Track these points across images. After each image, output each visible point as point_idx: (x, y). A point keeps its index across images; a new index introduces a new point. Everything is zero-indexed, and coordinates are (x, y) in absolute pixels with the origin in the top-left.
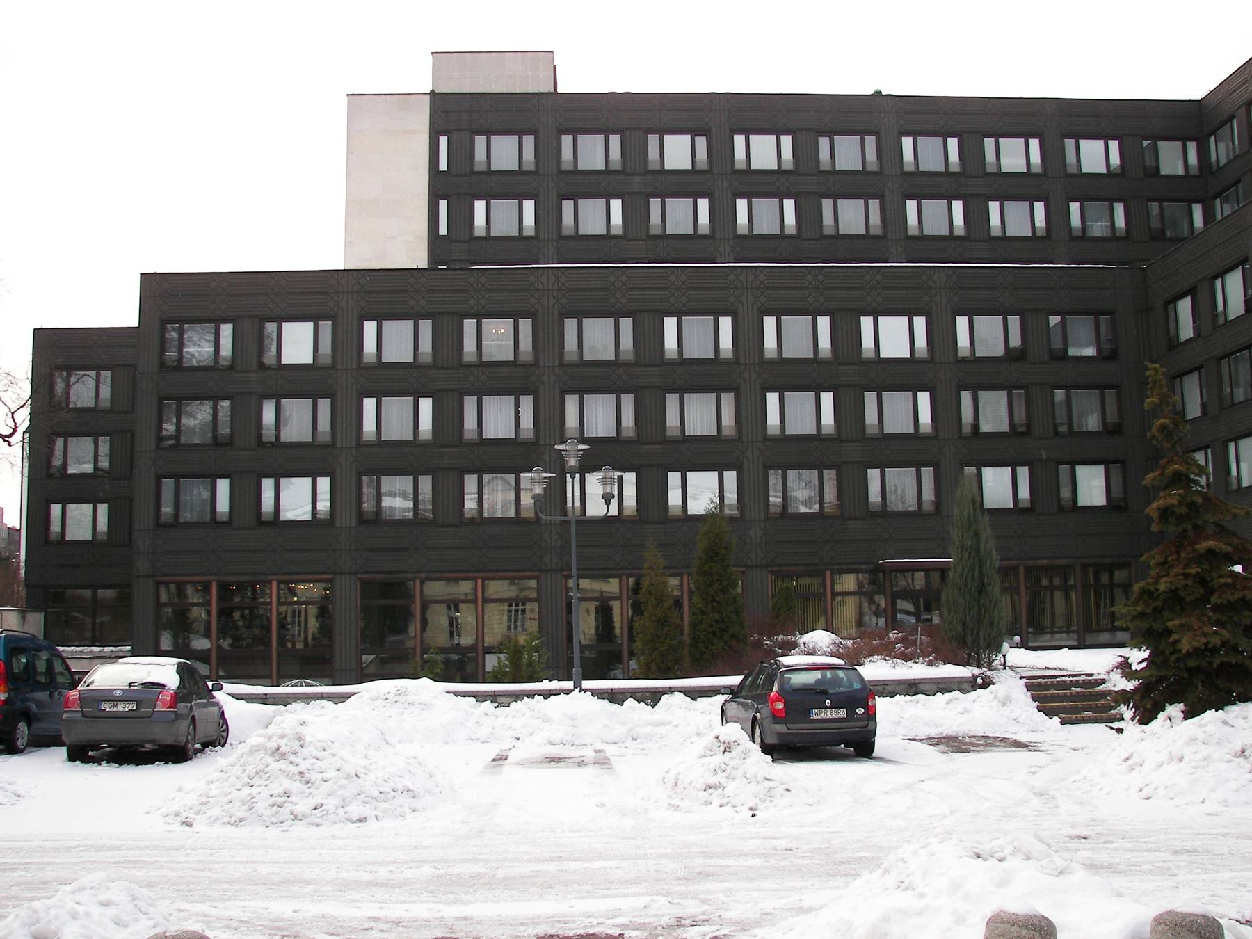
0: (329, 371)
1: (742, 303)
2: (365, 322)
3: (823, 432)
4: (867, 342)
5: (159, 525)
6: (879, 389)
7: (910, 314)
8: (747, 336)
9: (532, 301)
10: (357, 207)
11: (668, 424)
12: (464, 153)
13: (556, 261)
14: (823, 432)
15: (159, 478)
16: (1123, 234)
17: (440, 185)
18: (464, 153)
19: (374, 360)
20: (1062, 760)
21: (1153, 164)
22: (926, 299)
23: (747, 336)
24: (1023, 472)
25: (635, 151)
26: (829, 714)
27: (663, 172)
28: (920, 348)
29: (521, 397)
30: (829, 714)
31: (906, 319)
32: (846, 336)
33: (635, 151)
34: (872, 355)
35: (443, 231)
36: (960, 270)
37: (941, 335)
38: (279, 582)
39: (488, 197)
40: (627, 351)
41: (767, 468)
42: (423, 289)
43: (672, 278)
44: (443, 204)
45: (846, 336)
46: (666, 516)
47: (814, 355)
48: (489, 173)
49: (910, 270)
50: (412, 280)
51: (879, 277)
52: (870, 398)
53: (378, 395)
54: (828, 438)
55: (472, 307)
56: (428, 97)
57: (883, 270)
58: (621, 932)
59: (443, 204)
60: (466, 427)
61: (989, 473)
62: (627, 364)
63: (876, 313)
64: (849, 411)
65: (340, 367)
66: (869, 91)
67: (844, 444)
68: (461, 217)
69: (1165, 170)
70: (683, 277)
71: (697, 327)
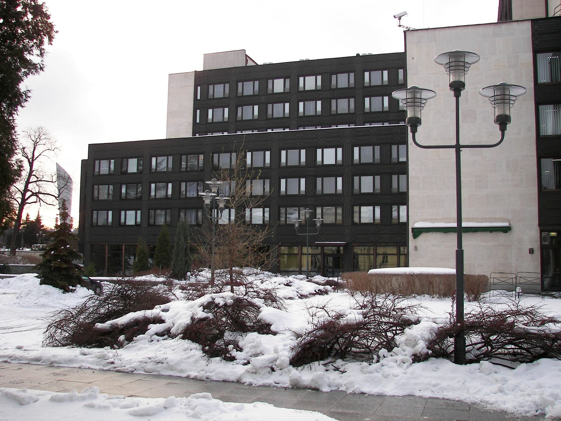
3: (338, 193)
5: (149, 225)
6: (322, 177)
8: (276, 158)
10: (171, 114)
13: (296, 128)
14: (338, 193)
15: (149, 210)
18: (205, 92)
19: (358, 162)
20: (178, 313)
22: (342, 141)
23: (276, 158)
25: (264, 87)
27: (273, 94)
29: (266, 180)
32: (311, 156)
33: (326, 82)
35: (198, 121)
36: (326, 131)
37: (348, 155)
38: (108, 245)
43: (341, 133)
45: (311, 156)
48: (214, 99)
49: (336, 130)
51: (324, 133)
52: (319, 180)
53: (286, 178)
54: (302, 196)
56: (194, 73)
57: (401, 127)
58: (393, 377)
59: (198, 111)
60: (317, 189)
61: (363, 209)
62: (378, 164)
63: (323, 147)
64: (311, 185)
67: (307, 198)
68: (204, 115)
70: (302, 135)
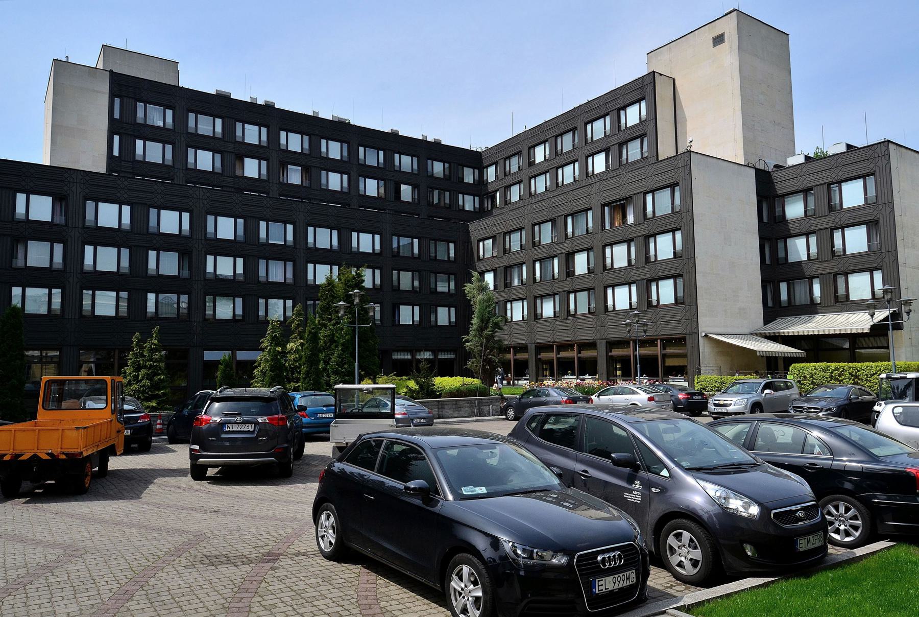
0: (64, 228)
1: (299, 219)
2: (31, 195)
4: (310, 239)
7: (180, 210)
9: (191, 204)
11: (85, 263)
12: (129, 112)
16: (448, 206)
17: (114, 127)
21: (462, 177)
24: (417, 309)
26: (697, 398)
28: (185, 230)
30: (697, 398)
31: (371, 235)
34: (312, 246)
39: (145, 139)
40: (153, 227)
41: (206, 294)
42: (126, 188)
44: (116, 138)
46: (258, 320)
47: (119, 226)
50: (330, 210)
55: (356, 227)
59: (116, 138)
65: (70, 225)
66: (387, 130)
69: (466, 180)
71: (276, 227)
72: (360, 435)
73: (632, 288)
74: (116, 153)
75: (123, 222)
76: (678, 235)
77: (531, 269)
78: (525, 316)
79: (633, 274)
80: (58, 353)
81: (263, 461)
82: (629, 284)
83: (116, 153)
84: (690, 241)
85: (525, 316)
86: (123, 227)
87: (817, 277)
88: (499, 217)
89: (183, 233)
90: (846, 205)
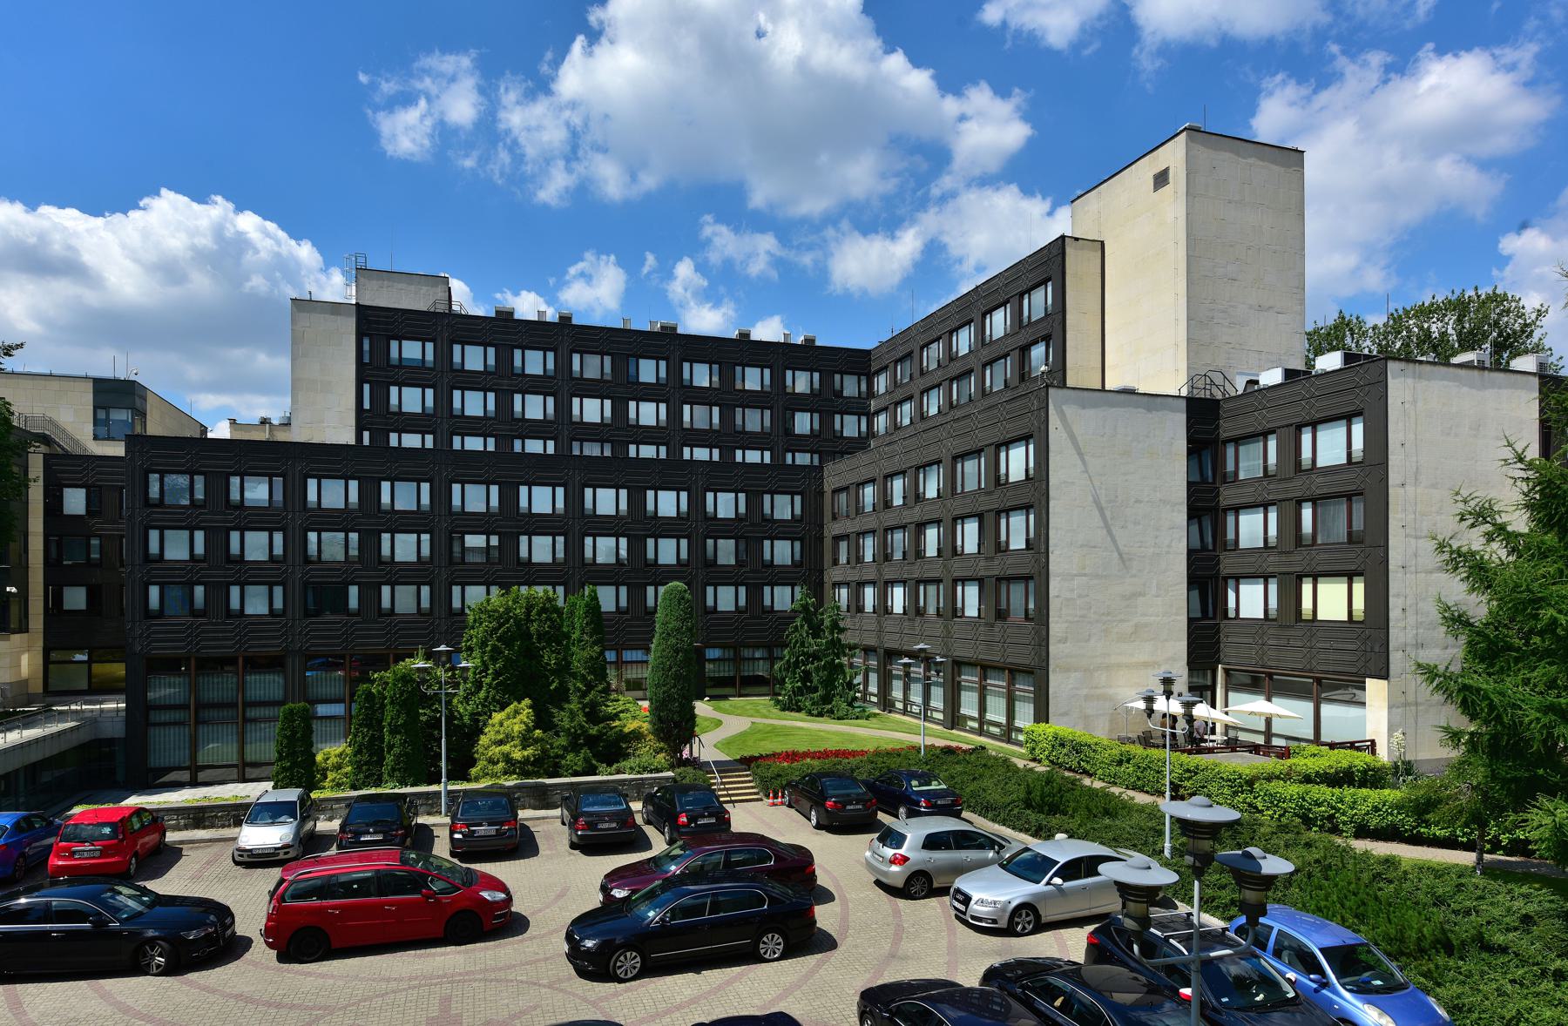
44: (367, 387)
59: (367, 387)
72: (783, 710)
73: (1354, 506)
74: (367, 405)
75: (491, 504)
76: (1358, 429)
77: (950, 592)
78: (1031, 472)
79: (1274, 490)
80: (151, 695)
81: (353, 903)
82: (1265, 506)
83: (367, 405)
84: (1043, 525)
85: (1031, 472)
86: (491, 511)
87: (1274, 504)
88: (1021, 402)
89: (422, 509)
90: (927, 555)
